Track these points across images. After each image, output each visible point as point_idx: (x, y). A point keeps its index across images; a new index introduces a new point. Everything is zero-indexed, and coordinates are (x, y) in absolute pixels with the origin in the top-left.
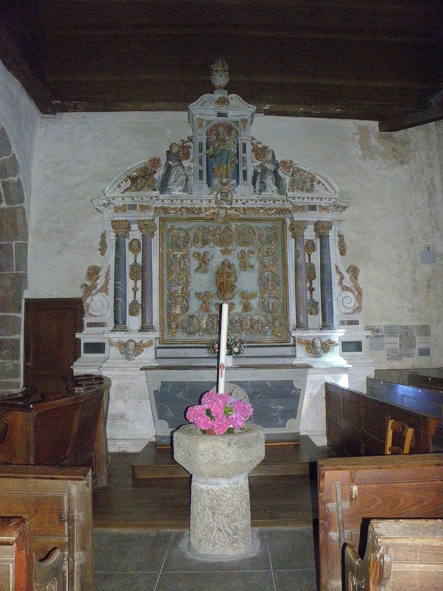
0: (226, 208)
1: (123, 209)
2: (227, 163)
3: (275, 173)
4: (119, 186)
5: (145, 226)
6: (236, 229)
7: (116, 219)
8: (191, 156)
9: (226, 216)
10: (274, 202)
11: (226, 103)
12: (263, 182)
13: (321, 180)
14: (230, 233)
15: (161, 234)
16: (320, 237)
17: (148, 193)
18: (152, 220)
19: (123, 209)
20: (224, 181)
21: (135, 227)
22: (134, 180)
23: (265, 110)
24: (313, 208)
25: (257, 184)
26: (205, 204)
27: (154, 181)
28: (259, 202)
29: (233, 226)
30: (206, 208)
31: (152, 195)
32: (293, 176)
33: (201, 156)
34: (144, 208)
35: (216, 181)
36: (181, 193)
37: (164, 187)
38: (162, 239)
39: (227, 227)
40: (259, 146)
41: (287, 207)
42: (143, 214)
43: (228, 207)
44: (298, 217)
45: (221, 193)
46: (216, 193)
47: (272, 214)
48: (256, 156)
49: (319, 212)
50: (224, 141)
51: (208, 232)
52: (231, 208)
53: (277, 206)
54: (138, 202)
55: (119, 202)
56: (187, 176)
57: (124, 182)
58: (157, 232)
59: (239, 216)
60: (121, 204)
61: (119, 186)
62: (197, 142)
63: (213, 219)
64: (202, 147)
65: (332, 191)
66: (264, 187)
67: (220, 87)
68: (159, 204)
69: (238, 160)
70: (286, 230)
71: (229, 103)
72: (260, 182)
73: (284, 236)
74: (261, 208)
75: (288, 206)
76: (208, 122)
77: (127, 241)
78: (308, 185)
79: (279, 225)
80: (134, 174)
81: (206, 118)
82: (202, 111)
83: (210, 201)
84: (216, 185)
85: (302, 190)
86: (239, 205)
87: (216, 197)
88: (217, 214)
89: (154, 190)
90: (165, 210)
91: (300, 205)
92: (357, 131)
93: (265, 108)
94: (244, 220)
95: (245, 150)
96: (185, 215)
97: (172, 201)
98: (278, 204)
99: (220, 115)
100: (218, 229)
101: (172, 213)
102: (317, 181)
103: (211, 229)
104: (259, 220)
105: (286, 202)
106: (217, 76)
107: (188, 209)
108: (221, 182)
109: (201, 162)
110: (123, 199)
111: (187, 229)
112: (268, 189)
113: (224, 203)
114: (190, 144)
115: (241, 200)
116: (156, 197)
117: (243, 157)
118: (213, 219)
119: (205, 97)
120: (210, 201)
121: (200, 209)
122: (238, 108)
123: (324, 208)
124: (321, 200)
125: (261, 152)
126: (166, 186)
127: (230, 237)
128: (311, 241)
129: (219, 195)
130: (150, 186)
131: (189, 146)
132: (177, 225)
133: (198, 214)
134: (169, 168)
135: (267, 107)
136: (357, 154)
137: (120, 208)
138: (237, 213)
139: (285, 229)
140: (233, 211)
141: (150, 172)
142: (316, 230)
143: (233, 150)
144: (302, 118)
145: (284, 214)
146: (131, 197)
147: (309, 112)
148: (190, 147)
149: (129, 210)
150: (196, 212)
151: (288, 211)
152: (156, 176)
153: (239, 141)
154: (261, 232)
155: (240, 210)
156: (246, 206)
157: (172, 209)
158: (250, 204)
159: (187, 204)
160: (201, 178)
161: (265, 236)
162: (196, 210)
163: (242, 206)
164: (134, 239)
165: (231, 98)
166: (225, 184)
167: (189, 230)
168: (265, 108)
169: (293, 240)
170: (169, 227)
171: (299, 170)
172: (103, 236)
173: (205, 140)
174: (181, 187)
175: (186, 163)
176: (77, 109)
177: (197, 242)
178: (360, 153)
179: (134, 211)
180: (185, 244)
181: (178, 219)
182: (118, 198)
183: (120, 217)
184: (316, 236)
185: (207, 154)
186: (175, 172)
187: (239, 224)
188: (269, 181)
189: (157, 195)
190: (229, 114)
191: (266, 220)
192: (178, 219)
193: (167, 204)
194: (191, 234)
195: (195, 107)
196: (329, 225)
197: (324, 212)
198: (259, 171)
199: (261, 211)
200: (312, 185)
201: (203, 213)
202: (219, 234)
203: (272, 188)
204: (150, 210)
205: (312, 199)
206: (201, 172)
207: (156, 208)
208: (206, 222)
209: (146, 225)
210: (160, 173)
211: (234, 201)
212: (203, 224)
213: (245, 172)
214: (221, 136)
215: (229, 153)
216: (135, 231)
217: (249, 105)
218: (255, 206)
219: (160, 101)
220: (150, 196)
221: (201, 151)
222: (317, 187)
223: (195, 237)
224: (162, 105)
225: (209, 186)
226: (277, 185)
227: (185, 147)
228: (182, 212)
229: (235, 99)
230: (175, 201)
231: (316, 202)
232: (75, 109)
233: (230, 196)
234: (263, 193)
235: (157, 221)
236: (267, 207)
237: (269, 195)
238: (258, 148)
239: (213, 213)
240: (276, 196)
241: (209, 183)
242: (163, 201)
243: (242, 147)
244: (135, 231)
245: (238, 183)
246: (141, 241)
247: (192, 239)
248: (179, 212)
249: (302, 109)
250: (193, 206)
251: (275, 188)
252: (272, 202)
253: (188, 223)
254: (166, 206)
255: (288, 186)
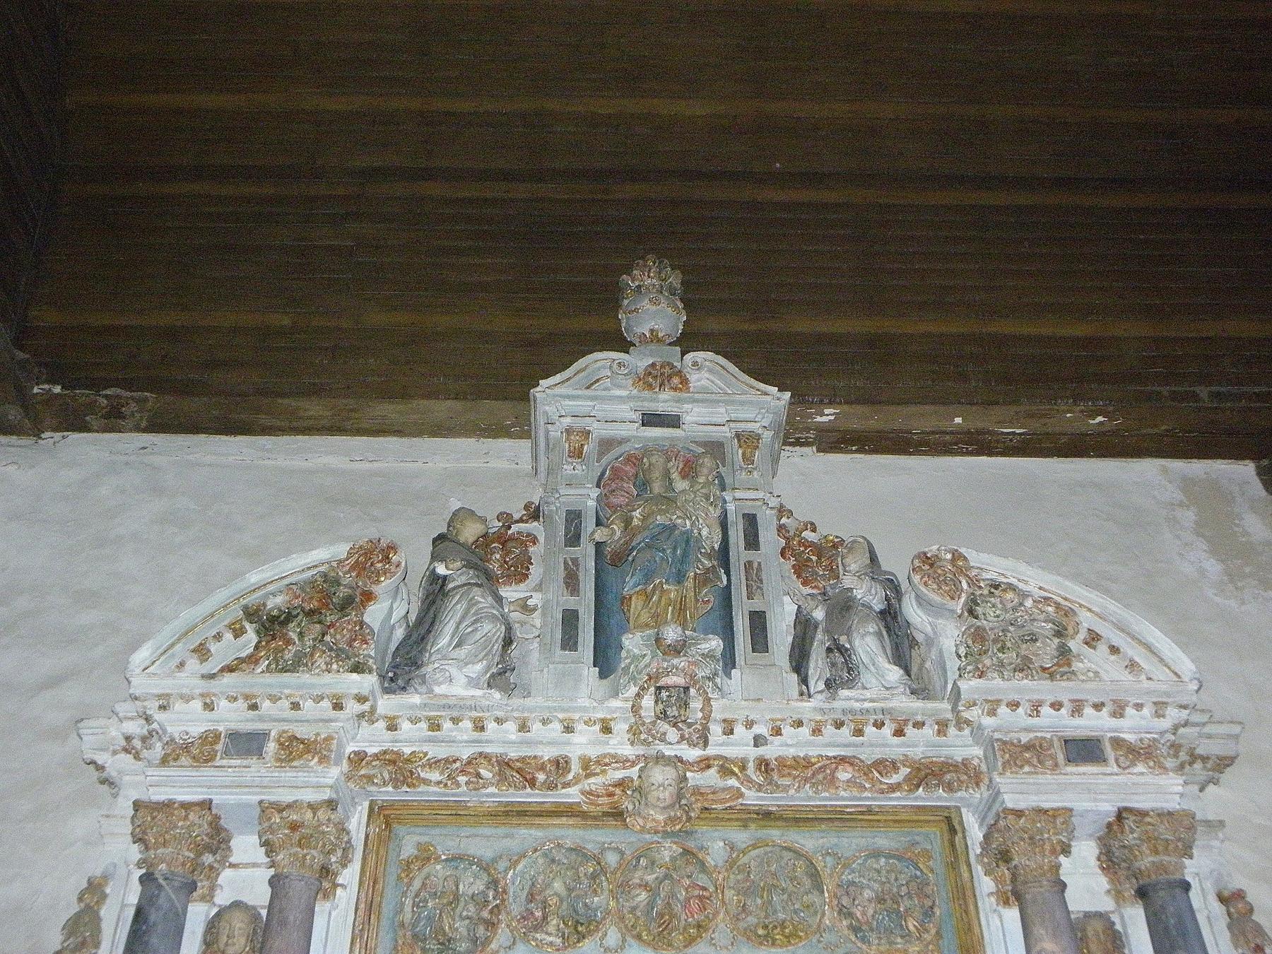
0: (680, 760)
1: (203, 750)
2: (680, 578)
3: (890, 617)
4: (202, 651)
5: (284, 828)
6: (731, 864)
7: (159, 795)
8: (536, 571)
9: (680, 796)
10: (899, 733)
11: (676, 380)
12: (841, 650)
13: (1101, 628)
14: (702, 880)
15: (371, 882)
16: (1142, 894)
17: (328, 678)
18: (331, 804)
19: (203, 750)
20: (672, 634)
21: (246, 846)
22: (272, 625)
23: (822, 430)
24: (1085, 750)
25: (812, 665)
26: (583, 744)
27: (362, 633)
28: (829, 730)
29: (714, 845)
30: (586, 763)
31: (338, 690)
32: (971, 612)
33: (575, 561)
34: (296, 749)
35: (633, 643)
36: (479, 693)
37: (404, 667)
38: (368, 909)
39: (686, 852)
40: (808, 535)
41: (958, 755)
42: (288, 775)
43: (692, 754)
44: (1021, 791)
45: (659, 689)
46: (633, 690)
47: (894, 788)
48: (798, 571)
49: (1116, 769)
50: (669, 500)
51: (594, 877)
52: (705, 764)
53: (917, 753)
54: (274, 717)
55: (187, 721)
56: (509, 629)
57: (229, 636)
58: (350, 876)
59: (742, 795)
60: (196, 730)
61: (202, 651)
62: (557, 511)
63: (617, 814)
64: (578, 527)
65: (1160, 673)
66: (845, 671)
67: (655, 338)
68: (371, 739)
69: (728, 573)
70: (969, 865)
71: (685, 381)
72: (829, 650)
73: (963, 895)
74: (843, 760)
75: (962, 747)
76: (607, 444)
77: (197, 915)
78: (1046, 652)
79: (933, 839)
80: (276, 602)
81: (599, 430)
82: (583, 406)
83: (607, 730)
84: (635, 658)
85: (1024, 667)
86: (740, 746)
87: (635, 709)
88: (639, 790)
89: (357, 668)
90: (400, 768)
91: (1025, 738)
92: (1179, 496)
93: (819, 419)
94: (766, 816)
95: (757, 535)
96: (493, 795)
97: (435, 726)
98: (920, 744)
99: (651, 420)
100: (643, 862)
101: (427, 782)
102: (1082, 635)
103: (612, 859)
104: (838, 818)
105: (952, 731)
106: (645, 304)
107: (504, 764)
108: (658, 640)
109: (572, 582)
110: (209, 707)
111: (494, 860)
112: (867, 678)
113: (673, 734)
114: (533, 527)
115: (749, 724)
116: (361, 699)
117: (748, 565)
118: (617, 814)
119: (601, 360)
120: (607, 730)
121: (561, 765)
122: (724, 400)
123: (1134, 753)
124: (1118, 712)
125: (813, 558)
126: (416, 664)
127: (700, 898)
128: (1099, 915)
129: (648, 701)
130: (339, 654)
131: (529, 535)
132: (447, 841)
133: (551, 786)
134: (436, 591)
135: (828, 415)
136: (1202, 572)
137: (186, 748)
138: (733, 782)
139: (962, 859)
140: (711, 778)
141: (343, 592)
142: (1110, 861)
143: (710, 536)
144: (958, 459)
145: (950, 788)
146: (247, 697)
147: (989, 432)
148: (534, 540)
149: (227, 753)
150: (541, 777)
151: (967, 774)
152: (374, 615)
153: (731, 507)
154: (846, 877)
155: (743, 768)
156: (771, 751)
157: (434, 764)
158: (792, 744)
159: (503, 739)
160: (570, 641)
161: (867, 894)
162: (542, 768)
163: (752, 753)
164: (237, 905)
165: (695, 364)
166: (677, 649)
167: (502, 865)
168: (819, 419)
169: (1012, 915)
170: (408, 850)
171: (996, 587)
172: (95, 890)
173: (592, 504)
174: (479, 667)
175: (511, 593)
176: (121, 416)
177: (540, 925)
178: (1213, 567)
179: (253, 761)
180: (481, 931)
181: (457, 814)
182: (187, 699)
183: (182, 785)
184: (1118, 895)
185: (599, 546)
186: (461, 609)
187: (741, 837)
188: (867, 645)
189: (365, 692)
190: (687, 419)
191: (866, 818)
192: (457, 814)
193: (410, 738)
194: (514, 880)
195: (558, 390)
196: (1181, 831)
197: (1140, 768)
198: (819, 614)
199: (844, 775)
200: (1064, 653)
201: (577, 780)
202: (645, 886)
203: (880, 675)
204: (324, 759)
205: (1077, 709)
206: (570, 619)
207: (359, 758)
208: (585, 827)
209: (294, 827)
210: (388, 611)
211: (716, 730)
212: (571, 834)
213: (758, 622)
214: (657, 488)
215: (687, 542)
216: (246, 866)
217: (762, 386)
218: (813, 752)
219: (432, 395)
220: (330, 699)
221: (573, 539)
222: (1091, 660)
223: (531, 898)
224: (442, 408)
225: (603, 675)
226: (900, 659)
227: (511, 539)
228: (478, 775)
229: (706, 369)
230: (447, 725)
231: (1093, 723)
232: (113, 420)
233: (696, 704)
234: (844, 693)
235: (357, 823)
236: (868, 755)
237: (872, 701)
238: (805, 544)
239: (621, 784)
240: (905, 703)
241: (605, 660)
242: (392, 727)
243: (741, 527)
244: (246, 866)
245: (729, 661)
246: (264, 913)
247: (516, 908)
248: (462, 779)
249: (958, 420)
250: (528, 752)
251: (894, 674)
252: (887, 731)
253: (501, 831)
254: (407, 751)
255: (953, 665)
